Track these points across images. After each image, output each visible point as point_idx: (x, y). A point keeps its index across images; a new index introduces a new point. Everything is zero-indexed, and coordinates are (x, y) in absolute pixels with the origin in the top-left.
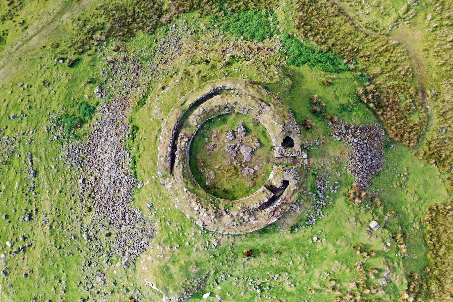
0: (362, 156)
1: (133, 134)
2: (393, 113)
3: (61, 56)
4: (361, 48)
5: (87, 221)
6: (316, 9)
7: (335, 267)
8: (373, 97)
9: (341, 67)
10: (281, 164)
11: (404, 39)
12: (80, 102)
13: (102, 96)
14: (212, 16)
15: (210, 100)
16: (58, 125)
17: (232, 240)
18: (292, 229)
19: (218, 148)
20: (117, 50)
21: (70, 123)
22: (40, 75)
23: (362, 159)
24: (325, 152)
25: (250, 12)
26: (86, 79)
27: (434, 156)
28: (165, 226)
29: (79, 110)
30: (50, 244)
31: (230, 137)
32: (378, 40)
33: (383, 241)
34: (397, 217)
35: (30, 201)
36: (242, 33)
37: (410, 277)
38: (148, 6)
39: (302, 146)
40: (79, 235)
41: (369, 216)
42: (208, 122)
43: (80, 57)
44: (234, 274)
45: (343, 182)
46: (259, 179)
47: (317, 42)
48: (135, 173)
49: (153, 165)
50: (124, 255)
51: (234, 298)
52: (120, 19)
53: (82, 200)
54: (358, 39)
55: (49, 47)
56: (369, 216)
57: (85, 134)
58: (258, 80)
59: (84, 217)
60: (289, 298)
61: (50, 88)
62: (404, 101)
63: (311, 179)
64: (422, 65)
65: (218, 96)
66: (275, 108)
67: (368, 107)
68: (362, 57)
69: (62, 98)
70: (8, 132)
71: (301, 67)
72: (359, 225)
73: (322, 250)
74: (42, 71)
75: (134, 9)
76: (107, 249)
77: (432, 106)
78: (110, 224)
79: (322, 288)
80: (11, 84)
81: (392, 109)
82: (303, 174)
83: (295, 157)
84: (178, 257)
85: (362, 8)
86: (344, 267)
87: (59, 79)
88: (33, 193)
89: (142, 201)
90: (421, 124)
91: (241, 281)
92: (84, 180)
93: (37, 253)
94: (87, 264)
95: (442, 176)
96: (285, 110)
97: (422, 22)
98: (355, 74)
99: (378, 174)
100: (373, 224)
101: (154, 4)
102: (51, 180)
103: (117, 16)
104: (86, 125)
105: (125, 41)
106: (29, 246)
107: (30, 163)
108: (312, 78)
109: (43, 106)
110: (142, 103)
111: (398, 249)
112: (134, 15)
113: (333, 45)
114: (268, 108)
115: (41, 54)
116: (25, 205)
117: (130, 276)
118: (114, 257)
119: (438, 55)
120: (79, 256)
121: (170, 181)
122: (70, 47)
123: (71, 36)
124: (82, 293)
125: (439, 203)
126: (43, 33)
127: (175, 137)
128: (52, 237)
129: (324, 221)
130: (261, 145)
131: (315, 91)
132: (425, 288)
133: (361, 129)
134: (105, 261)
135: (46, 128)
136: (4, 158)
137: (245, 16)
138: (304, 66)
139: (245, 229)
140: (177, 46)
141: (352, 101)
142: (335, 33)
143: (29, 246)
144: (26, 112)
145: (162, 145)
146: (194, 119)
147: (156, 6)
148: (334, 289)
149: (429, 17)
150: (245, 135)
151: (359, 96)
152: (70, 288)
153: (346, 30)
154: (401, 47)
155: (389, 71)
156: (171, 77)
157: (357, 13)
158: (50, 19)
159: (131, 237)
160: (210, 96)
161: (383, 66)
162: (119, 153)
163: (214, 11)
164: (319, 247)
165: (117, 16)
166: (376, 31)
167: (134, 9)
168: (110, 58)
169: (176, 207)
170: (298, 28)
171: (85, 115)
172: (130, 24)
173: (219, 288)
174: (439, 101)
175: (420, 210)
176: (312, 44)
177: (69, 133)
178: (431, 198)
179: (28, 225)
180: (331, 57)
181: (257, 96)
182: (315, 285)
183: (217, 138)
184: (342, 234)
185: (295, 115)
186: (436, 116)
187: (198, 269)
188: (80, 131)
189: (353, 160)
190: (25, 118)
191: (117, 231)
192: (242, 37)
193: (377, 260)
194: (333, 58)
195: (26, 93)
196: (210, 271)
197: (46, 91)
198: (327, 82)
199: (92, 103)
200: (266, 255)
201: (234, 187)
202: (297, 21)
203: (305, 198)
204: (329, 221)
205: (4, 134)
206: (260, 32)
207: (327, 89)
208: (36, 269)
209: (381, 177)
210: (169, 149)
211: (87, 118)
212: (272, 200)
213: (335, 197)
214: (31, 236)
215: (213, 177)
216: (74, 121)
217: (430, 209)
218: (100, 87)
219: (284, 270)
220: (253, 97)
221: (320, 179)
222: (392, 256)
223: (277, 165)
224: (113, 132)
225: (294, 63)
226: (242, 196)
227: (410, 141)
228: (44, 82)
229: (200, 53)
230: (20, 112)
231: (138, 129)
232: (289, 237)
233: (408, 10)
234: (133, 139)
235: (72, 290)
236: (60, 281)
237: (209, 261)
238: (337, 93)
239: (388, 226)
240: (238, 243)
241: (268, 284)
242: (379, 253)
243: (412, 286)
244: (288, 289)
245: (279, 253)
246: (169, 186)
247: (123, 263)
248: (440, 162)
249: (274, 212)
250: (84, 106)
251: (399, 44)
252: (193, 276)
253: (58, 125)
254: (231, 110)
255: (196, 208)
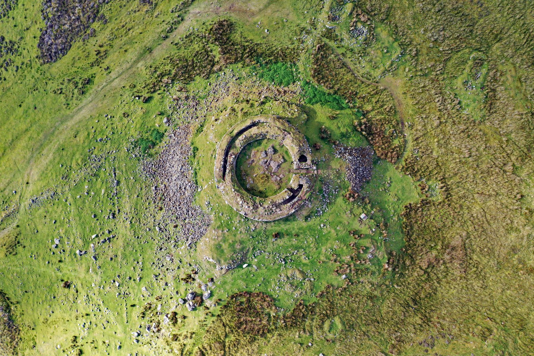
0: (356, 169)
1: (194, 153)
2: (380, 138)
3: (137, 94)
4: (358, 91)
5: (159, 217)
6: (327, 63)
7: (336, 245)
8: (365, 127)
9: (344, 105)
10: (298, 173)
11: (389, 86)
12: (152, 129)
13: (169, 125)
14: (251, 67)
15: (250, 130)
16: (135, 146)
17: (264, 226)
18: (306, 218)
19: (255, 162)
20: (180, 90)
21: (145, 145)
22: (121, 108)
23: (355, 171)
24: (329, 165)
25: (279, 64)
26: (157, 112)
27: (409, 169)
28: (218, 217)
29: (151, 135)
30: (129, 234)
31: (263, 155)
32: (370, 86)
33: (370, 228)
34: (381, 212)
35: (114, 203)
36: (273, 80)
37: (390, 254)
38: (203, 57)
39: (312, 161)
40: (153, 228)
41: (360, 210)
42: (250, 144)
43: (152, 95)
44: (266, 250)
45: (342, 187)
46: (283, 184)
47: (327, 87)
48: (196, 181)
49: (209, 174)
50: (187, 240)
51: (266, 268)
52: (183, 67)
53: (155, 202)
54: (356, 85)
55: (128, 87)
56: (360, 210)
57: (156, 153)
58: (283, 115)
59: (156, 215)
60: (304, 268)
61: (129, 119)
62: (388, 130)
63: (318, 185)
64: (402, 104)
65: (255, 127)
66: (294, 135)
67: (362, 134)
68: (359, 98)
69: (138, 126)
70: (96, 152)
71: (315, 106)
72: (353, 216)
73: (327, 234)
74: (122, 105)
75: (193, 60)
76: (175, 237)
77: (409, 133)
78: (177, 218)
79: (327, 260)
80: (98, 115)
81: (379, 136)
82: (312, 180)
83: (308, 169)
84: (227, 238)
85: (359, 63)
86: (342, 245)
87: (135, 112)
88: (116, 198)
89: (202, 200)
90: (400, 147)
91: (271, 255)
92: (156, 187)
93: (120, 242)
94: (159, 249)
95: (415, 184)
96: (300, 137)
97: (402, 73)
98: (353, 110)
99: (368, 182)
100: (363, 216)
101: (208, 57)
102: (130, 187)
103: (180, 65)
104: (157, 147)
105: (187, 84)
106: (113, 237)
107: (114, 175)
108: (322, 114)
109: (123, 132)
110: (200, 130)
111: (381, 234)
112: (193, 65)
113: (338, 89)
114: (289, 135)
115: (121, 92)
116: (110, 207)
117: (192, 255)
118: (180, 243)
119: (413, 97)
120: (152, 243)
121: (222, 185)
122: (144, 87)
123: (145, 79)
124: (154, 271)
125: (412, 203)
126: (123, 76)
127: (226, 154)
128: (132, 230)
129: (328, 213)
130: (285, 161)
131: (324, 123)
132: (401, 262)
133: (356, 150)
134: (173, 246)
135: (126, 149)
136: (93, 172)
137: (275, 67)
138: (317, 104)
139: (273, 217)
140: (226, 89)
141: (350, 130)
142: (340, 80)
143: (113, 237)
144: (110, 136)
145: (217, 160)
146: (239, 143)
147: (210, 58)
148: (335, 261)
149: (407, 70)
150: (274, 154)
151: (355, 127)
152: (145, 267)
153: (348, 79)
154: (387, 91)
155: (378, 109)
156: (222, 112)
157: (356, 66)
158: (128, 66)
159: (193, 227)
160: (250, 127)
161: (374, 104)
162: (184, 167)
163: (253, 63)
164: (325, 231)
165: (180, 65)
166: (370, 80)
167: (193, 60)
168: (174, 97)
169: (226, 203)
170: (314, 77)
171: (156, 139)
172: (189, 71)
173: (256, 260)
174: (413, 130)
175: (399, 207)
176: (323, 88)
177: (144, 152)
178: (407, 199)
179: (112, 223)
180: (337, 98)
181: (282, 127)
182: (322, 258)
183: (255, 155)
184: (341, 222)
185: (308, 140)
186: (411, 140)
187: (242, 246)
188: (153, 151)
189: (349, 171)
190: (109, 141)
191: (182, 223)
192: (273, 83)
193: (365, 240)
194: (339, 98)
195: (109, 122)
196: (249, 248)
197: (125, 120)
198: (332, 117)
199: (162, 130)
200: (288, 237)
201: (266, 189)
202: (312, 72)
203: (315, 197)
204: (332, 214)
205: (92, 153)
206: (286, 79)
207: (332, 122)
208: (119, 254)
209: (371, 184)
210: (222, 163)
211: (158, 141)
212: (292, 198)
213: (336, 197)
214: (114, 230)
215: (252, 182)
216: (149, 143)
217: (406, 207)
218: (168, 119)
219: (301, 247)
220: (279, 128)
221: (325, 184)
222: (377, 238)
223: (296, 174)
224: (178, 152)
225: (310, 102)
226: (272, 195)
227: (392, 158)
228: (124, 114)
229: (242, 94)
230: (105, 137)
231: (197, 149)
232: (304, 224)
233: (392, 65)
234: (194, 156)
235: (147, 269)
236: (138, 262)
237: (249, 240)
238: (339, 125)
239: (374, 217)
240: (269, 228)
241: (290, 258)
242: (366, 236)
243: (391, 260)
244: (304, 261)
245: (297, 235)
246: (222, 188)
247: (187, 245)
248: (414, 173)
249: (293, 205)
250: (156, 132)
251: (385, 89)
252: (238, 251)
253: (135, 146)
254: (264, 137)
255: (241, 202)
